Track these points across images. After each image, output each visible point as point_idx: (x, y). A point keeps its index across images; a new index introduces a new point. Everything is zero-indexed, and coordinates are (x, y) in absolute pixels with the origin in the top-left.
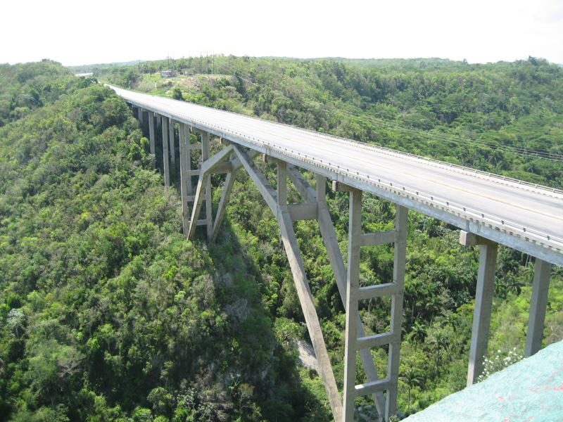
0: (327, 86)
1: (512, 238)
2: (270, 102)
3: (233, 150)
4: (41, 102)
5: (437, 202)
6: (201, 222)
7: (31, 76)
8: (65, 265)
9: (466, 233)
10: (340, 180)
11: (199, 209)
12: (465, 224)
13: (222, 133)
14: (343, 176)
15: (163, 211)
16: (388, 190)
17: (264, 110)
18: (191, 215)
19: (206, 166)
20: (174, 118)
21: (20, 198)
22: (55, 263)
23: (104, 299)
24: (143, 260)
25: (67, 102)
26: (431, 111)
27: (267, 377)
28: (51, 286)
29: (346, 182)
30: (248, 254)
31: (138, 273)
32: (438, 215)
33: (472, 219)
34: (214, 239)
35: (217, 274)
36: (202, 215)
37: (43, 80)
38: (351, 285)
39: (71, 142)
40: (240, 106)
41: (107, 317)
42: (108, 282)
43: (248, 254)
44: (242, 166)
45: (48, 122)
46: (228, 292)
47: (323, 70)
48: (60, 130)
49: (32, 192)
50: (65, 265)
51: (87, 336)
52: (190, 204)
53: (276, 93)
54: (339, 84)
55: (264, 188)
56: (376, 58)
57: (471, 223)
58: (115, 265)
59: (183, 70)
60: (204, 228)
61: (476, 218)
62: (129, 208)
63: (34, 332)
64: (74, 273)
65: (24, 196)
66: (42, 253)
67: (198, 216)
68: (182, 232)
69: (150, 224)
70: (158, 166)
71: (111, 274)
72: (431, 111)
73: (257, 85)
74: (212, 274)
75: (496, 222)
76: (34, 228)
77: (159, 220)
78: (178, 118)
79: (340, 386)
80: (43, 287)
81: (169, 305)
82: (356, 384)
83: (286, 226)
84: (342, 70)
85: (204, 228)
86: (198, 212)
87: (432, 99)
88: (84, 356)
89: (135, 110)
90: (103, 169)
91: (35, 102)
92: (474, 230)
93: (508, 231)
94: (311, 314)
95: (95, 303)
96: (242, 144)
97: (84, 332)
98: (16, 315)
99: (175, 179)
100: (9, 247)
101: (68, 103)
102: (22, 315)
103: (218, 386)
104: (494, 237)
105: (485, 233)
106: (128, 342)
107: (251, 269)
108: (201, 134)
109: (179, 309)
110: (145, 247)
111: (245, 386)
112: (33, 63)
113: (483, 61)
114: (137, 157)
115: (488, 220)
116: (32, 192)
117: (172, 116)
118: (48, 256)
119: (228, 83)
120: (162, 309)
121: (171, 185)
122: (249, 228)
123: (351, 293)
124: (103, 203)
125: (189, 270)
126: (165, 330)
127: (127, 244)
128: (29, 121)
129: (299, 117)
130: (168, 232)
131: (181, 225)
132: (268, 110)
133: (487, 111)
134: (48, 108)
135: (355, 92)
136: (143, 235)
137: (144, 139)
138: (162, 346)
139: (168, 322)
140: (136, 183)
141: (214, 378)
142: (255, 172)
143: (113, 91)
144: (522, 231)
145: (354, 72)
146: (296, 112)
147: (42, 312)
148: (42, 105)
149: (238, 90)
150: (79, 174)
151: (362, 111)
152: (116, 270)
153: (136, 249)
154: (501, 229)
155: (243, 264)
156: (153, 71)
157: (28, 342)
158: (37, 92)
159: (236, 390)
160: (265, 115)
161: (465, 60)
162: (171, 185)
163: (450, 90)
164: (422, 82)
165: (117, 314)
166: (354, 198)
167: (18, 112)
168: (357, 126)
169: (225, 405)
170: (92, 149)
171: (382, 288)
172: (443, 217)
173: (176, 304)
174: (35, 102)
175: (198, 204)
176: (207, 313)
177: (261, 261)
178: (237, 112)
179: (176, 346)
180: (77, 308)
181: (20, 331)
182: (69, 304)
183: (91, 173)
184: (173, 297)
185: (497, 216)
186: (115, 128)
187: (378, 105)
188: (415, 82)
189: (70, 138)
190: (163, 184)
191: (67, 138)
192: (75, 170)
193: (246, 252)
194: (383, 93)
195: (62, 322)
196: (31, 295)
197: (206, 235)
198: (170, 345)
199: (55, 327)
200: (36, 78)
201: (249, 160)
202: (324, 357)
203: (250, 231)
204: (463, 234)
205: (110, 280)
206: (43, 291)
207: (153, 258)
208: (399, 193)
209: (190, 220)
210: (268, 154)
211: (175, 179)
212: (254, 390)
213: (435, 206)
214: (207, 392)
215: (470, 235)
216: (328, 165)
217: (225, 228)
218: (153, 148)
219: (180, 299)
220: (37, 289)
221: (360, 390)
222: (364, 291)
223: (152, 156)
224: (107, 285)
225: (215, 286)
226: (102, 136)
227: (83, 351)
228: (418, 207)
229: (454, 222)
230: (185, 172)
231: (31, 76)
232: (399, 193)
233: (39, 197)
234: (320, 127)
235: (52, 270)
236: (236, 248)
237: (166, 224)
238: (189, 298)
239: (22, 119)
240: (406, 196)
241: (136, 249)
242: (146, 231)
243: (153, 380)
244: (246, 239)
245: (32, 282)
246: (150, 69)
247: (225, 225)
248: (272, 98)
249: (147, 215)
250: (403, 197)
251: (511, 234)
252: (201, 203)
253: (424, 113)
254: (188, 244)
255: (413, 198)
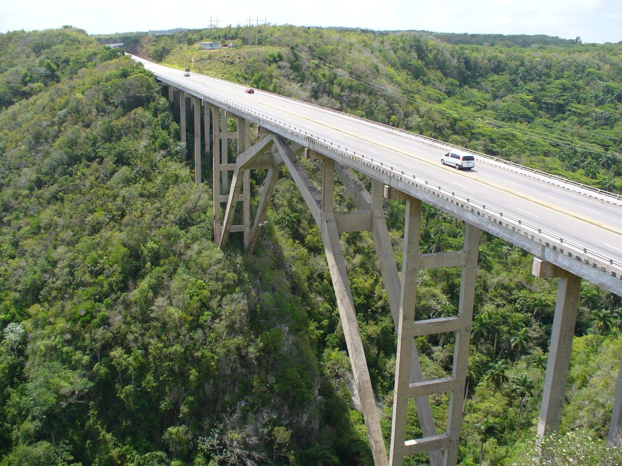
0: (405, 66)
1: (596, 271)
2: (333, 84)
3: (272, 142)
4: (57, 77)
5: (506, 219)
6: (235, 229)
7: (48, 46)
8: (71, 274)
9: (541, 261)
10: (394, 185)
11: (233, 212)
12: (540, 249)
13: (259, 120)
14: (398, 180)
15: (190, 212)
16: (450, 200)
17: (325, 92)
18: (223, 218)
19: (242, 159)
20: (207, 100)
21: (26, 192)
22: (62, 270)
23: (117, 320)
24: (164, 272)
25: (87, 76)
26: (531, 101)
27: (309, 422)
28: (55, 298)
29: (400, 186)
30: (294, 269)
31: (157, 289)
32: (508, 236)
33: (548, 245)
34: (252, 249)
35: (253, 293)
36: (237, 219)
37: (61, 51)
38: (404, 317)
39: (88, 126)
40: (295, 87)
41: (119, 340)
42: (122, 298)
43: (294, 269)
44: (283, 163)
45: (63, 101)
46: (266, 315)
47: (401, 45)
48: (77, 112)
49: (40, 184)
50: (71, 274)
51: (95, 359)
52: (224, 205)
53: (340, 72)
54: (420, 62)
55: (307, 191)
56: (470, 33)
57: (547, 249)
58: (133, 274)
59: (227, 42)
60: (240, 235)
61: (553, 243)
62: (149, 207)
63: (34, 353)
64: (83, 284)
65: (31, 189)
66: (47, 259)
67: (231, 221)
68: (213, 240)
69: (175, 229)
70: (189, 158)
71: (125, 288)
72: (531, 101)
73: (316, 62)
74: (247, 293)
75: (578, 251)
76: (39, 228)
77: (185, 224)
78: (212, 100)
79: (387, 438)
80: (46, 300)
81: (193, 328)
82: (407, 440)
83: (331, 239)
84: (425, 46)
85: (240, 235)
86: (232, 216)
87: (534, 85)
88: (91, 384)
89: (165, 89)
90: (121, 160)
91: (51, 77)
92: (551, 258)
93: (591, 262)
94: (356, 350)
95: (105, 322)
96: (286, 136)
97: (91, 355)
98: (14, 332)
99: (206, 176)
100: (11, 250)
101: (88, 80)
102: (22, 331)
103: (249, 429)
104: (575, 269)
105: (563, 262)
106: (142, 370)
107: (295, 289)
108: (241, 121)
109: (205, 333)
110: (167, 256)
111: (282, 429)
112: (52, 31)
113: (532, 34)
114: (164, 146)
115: (569, 245)
116: (40, 184)
117: (205, 97)
118: (54, 264)
119: (281, 58)
120: (184, 333)
121: (202, 181)
122: (298, 236)
123: (404, 328)
124: (119, 201)
125: (219, 286)
126: (187, 358)
127: (146, 252)
128: (43, 98)
129: (368, 101)
130: (195, 239)
131: (213, 231)
132: (330, 93)
133: (601, 103)
134: (64, 85)
135: (439, 74)
136: (165, 242)
137: (174, 126)
138: (183, 376)
139: (190, 348)
140: (160, 178)
141: (244, 420)
142: (297, 170)
143: (140, 63)
144: (609, 263)
145: (438, 50)
146: (363, 96)
147: (44, 329)
148: (58, 81)
149: (291, 68)
150: (95, 165)
151: (446, 96)
152: (130, 283)
153: (156, 259)
154: (583, 259)
155: (288, 283)
156: (191, 42)
157: (28, 365)
158: (55, 67)
159: (270, 434)
160: (325, 99)
161: (578, 38)
162: (202, 181)
163: (556, 75)
164: (522, 65)
165: (130, 337)
166: (411, 208)
167: (32, 89)
168: (437, 116)
169: (255, 455)
170: (111, 135)
171: (444, 322)
172: (514, 239)
173: (202, 327)
174: (51, 77)
175: (232, 206)
176: (239, 340)
177: (309, 278)
178: (289, 95)
179: (199, 378)
180: (84, 327)
181: (20, 350)
182: (75, 321)
183: (109, 163)
184: (198, 319)
185: (577, 239)
186: (140, 110)
187: (467, 90)
188: (514, 64)
189: (87, 120)
190: (193, 180)
191: (83, 121)
192: (90, 159)
193: (291, 266)
194: (474, 77)
195: (68, 342)
196: (34, 309)
197: (242, 245)
198: (192, 377)
199: (54, 348)
200: (53, 48)
201: (291, 155)
202: (370, 403)
203: (297, 242)
204: (537, 262)
205: (124, 294)
206: (46, 304)
207: (175, 270)
208: (462, 206)
209: (222, 224)
210: (311, 148)
211: (206, 176)
212: (292, 436)
213: (504, 225)
214: (235, 436)
215: (545, 264)
216: (380, 165)
217: (265, 236)
218: (184, 136)
219: (206, 321)
220: (39, 302)
221: (410, 446)
222: (420, 325)
223: (183, 144)
224: (119, 301)
225: (249, 307)
226: (123, 120)
227: (91, 379)
228: (485, 224)
229: (527, 246)
230: (219, 167)
231: (48, 46)
232: (462, 206)
233: (47, 192)
234: (393, 114)
235: (57, 279)
236: (279, 263)
237: (193, 229)
238: (217, 321)
239: (35, 97)
240: (470, 210)
241: (156, 259)
242: (168, 237)
243: (172, 417)
244: (288, 248)
245: (34, 293)
246: (188, 38)
247: (266, 232)
248: (335, 78)
249: (171, 217)
250: (468, 211)
251: (595, 266)
252: (235, 205)
253: (524, 103)
254: (219, 254)
255: (479, 213)
